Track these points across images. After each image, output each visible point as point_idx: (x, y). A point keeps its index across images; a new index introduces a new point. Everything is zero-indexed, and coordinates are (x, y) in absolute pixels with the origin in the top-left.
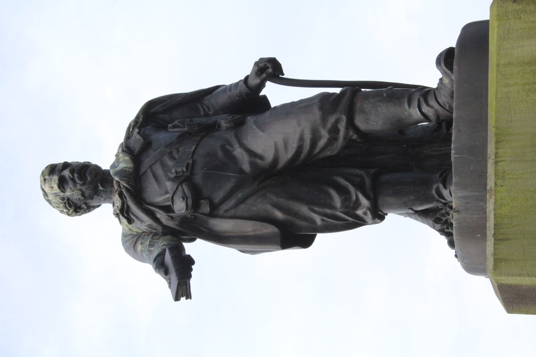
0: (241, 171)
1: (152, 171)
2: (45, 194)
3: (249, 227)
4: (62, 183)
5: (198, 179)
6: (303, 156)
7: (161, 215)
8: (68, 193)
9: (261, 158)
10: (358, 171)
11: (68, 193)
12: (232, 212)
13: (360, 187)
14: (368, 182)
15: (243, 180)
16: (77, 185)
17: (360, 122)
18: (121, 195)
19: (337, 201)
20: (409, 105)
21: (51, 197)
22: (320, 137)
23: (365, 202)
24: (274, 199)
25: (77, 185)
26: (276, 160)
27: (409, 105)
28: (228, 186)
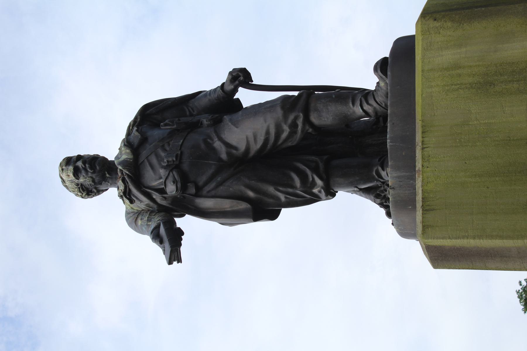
0: (220, 160)
1: (148, 161)
2: (63, 181)
3: (227, 204)
4: (76, 172)
5: (185, 166)
6: (269, 146)
7: (156, 196)
8: (81, 180)
9: (236, 148)
10: (313, 158)
11: (81, 180)
12: (213, 193)
13: (316, 170)
14: (321, 166)
15: (222, 166)
16: (88, 173)
17: (314, 119)
18: (124, 181)
19: (297, 182)
20: (353, 104)
21: (68, 184)
22: (283, 131)
23: (319, 182)
24: (247, 181)
25: (88, 173)
26: (248, 149)
27: (353, 104)
28: (210, 171)
